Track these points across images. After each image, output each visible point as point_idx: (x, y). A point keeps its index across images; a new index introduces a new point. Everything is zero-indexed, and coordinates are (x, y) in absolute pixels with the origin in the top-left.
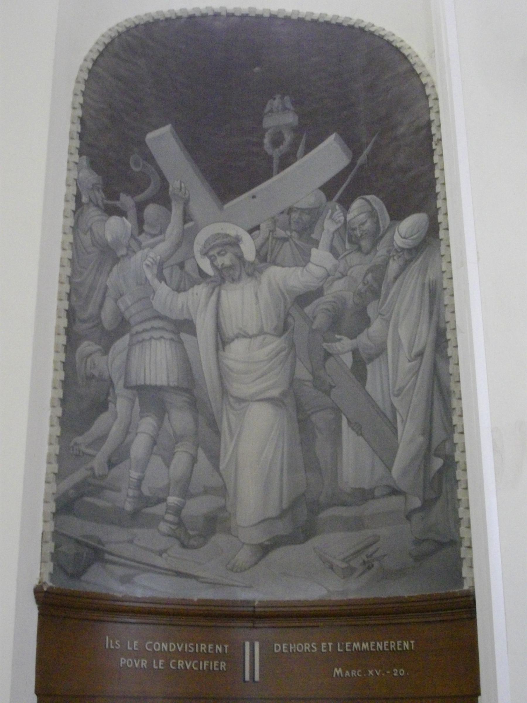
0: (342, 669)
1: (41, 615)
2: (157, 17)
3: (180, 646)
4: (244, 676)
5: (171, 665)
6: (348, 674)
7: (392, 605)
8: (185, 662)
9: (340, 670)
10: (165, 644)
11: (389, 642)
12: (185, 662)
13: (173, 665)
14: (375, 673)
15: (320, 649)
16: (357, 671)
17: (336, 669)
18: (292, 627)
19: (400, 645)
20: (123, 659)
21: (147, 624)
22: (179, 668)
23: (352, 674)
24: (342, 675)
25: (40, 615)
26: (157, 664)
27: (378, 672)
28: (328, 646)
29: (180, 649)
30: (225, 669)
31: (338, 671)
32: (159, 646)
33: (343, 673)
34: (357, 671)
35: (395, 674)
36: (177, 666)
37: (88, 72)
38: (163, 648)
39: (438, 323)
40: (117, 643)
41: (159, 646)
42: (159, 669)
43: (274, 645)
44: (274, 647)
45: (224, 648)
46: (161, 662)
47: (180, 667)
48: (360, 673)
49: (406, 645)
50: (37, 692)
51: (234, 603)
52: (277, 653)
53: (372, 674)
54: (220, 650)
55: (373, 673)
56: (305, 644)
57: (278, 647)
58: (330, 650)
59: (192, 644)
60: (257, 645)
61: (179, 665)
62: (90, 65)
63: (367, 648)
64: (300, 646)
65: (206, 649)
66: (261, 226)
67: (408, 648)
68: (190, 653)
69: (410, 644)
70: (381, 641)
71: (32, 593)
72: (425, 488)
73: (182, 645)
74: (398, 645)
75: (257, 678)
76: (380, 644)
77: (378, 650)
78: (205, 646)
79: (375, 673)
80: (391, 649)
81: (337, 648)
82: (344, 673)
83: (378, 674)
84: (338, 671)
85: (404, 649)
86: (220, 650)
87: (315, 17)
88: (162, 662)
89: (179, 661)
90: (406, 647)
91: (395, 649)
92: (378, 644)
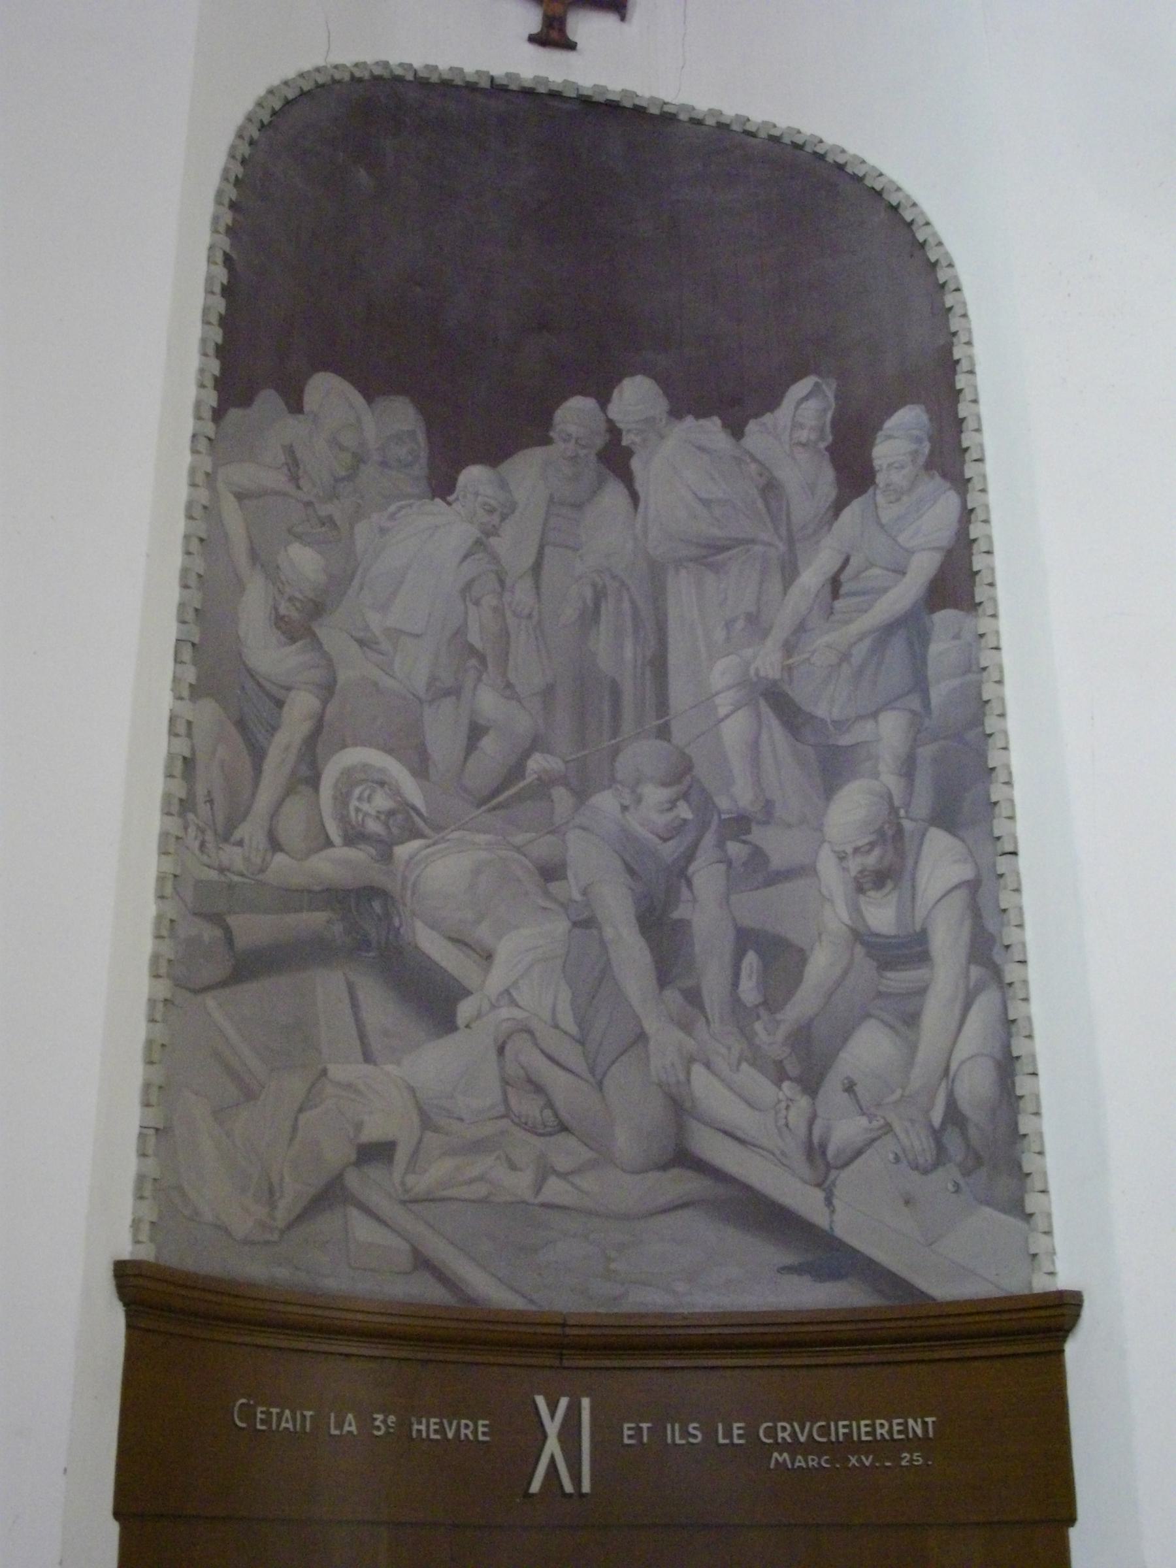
4: (561, 1487)
8: (793, 1427)
10: (916, 1422)
12: (793, 1427)
16: (820, 1458)
20: (467, 1422)
22: (879, 1437)
23: (811, 1463)
26: (728, 1434)
28: (639, 1430)
29: (450, 1435)
33: (790, 1460)
34: (820, 1458)
35: (904, 1463)
40: (692, 1431)
48: (827, 1461)
49: (914, 1425)
54: (919, 1431)
55: (857, 1461)
58: (645, 1439)
60: (677, 1426)
61: (879, 1431)
65: (887, 1432)
68: (693, 1444)
69: (925, 1424)
70: (792, 1420)
77: (911, 1435)
78: (887, 1425)
79: (859, 1460)
80: (879, 1437)
81: (329, 1428)
83: (867, 1464)
85: (911, 1435)
86: (919, 1431)
92: (911, 1422)
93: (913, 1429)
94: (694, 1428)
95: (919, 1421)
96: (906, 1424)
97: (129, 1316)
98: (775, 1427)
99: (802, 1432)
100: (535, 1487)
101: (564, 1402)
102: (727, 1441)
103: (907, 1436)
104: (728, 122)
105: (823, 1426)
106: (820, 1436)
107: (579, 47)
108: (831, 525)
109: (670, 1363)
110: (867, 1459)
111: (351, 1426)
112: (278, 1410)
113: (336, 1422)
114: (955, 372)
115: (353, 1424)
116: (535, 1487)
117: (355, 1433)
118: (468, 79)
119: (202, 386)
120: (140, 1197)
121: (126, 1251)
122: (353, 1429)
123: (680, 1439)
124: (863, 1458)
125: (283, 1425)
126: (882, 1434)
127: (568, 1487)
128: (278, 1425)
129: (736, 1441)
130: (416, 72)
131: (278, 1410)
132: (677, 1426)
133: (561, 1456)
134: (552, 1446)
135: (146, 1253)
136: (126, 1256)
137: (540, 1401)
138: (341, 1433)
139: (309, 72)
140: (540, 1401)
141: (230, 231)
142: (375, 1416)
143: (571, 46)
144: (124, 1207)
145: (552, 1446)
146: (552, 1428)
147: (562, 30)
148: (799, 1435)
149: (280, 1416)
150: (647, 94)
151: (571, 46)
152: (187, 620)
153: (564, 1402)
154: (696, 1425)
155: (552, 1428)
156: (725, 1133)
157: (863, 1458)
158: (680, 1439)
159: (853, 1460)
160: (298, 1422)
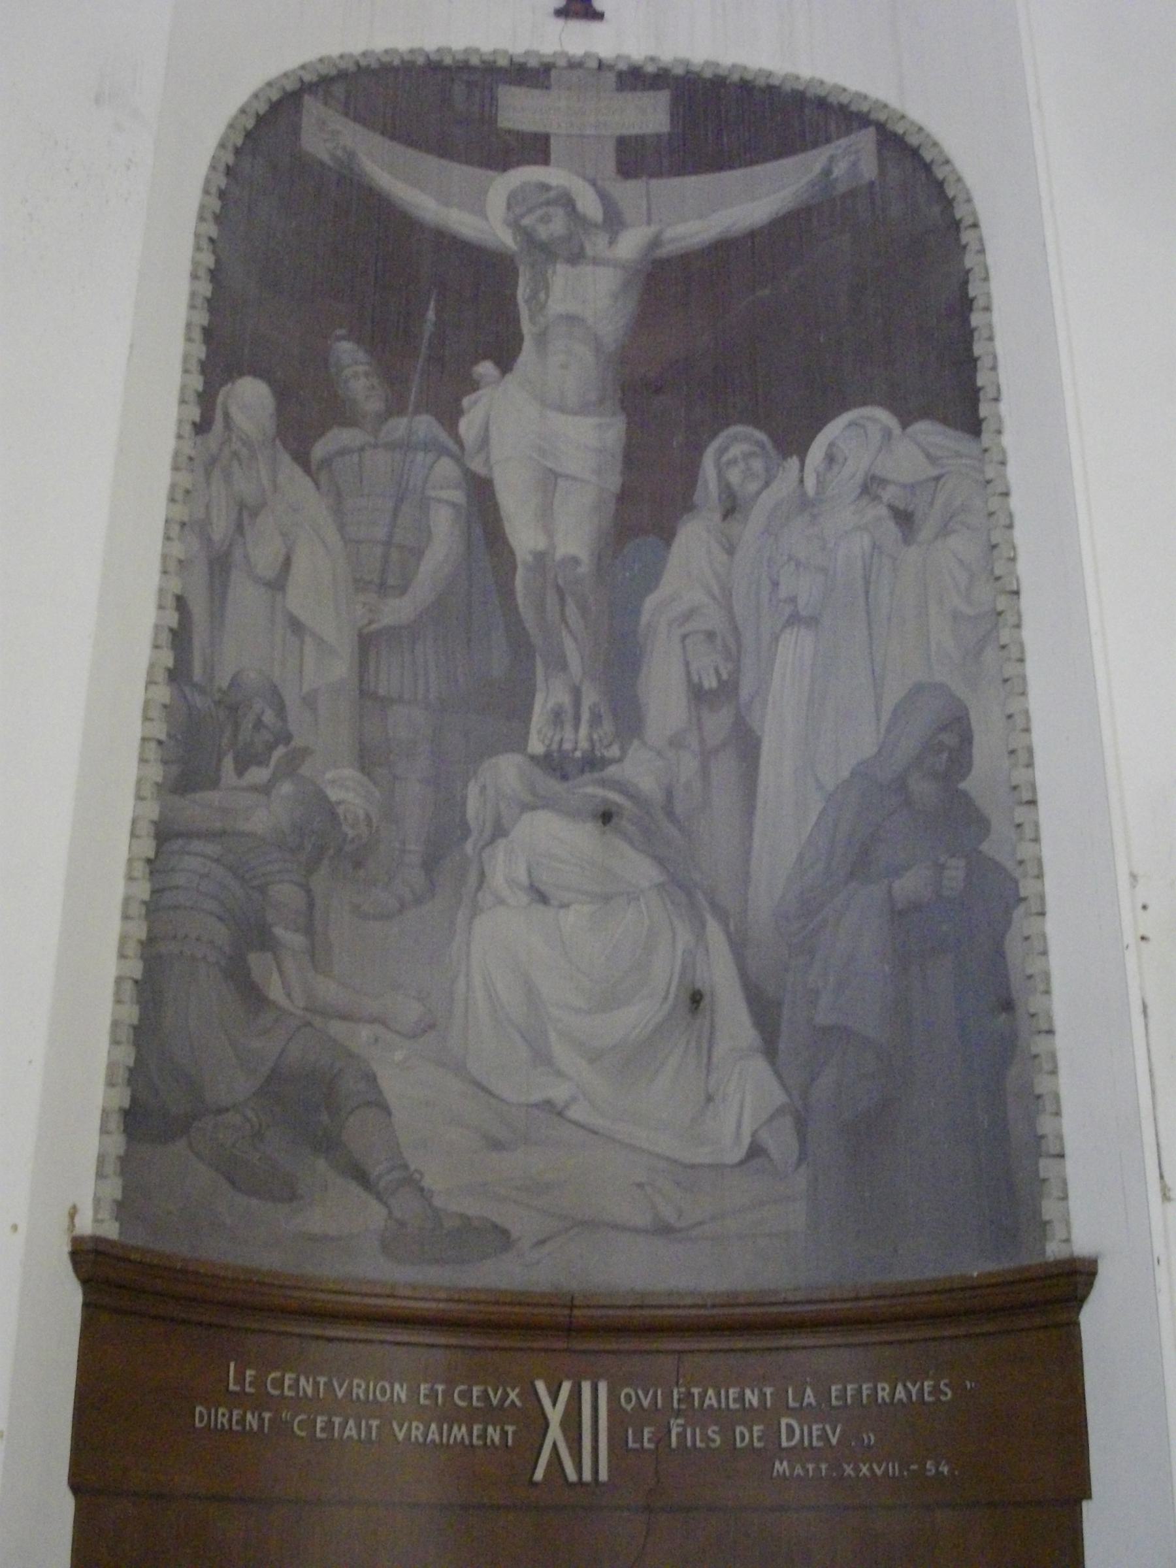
0: (789, 1461)
2: (343, 65)
5: (456, 1395)
6: (354, 1433)
9: (785, 1463)
11: (861, 1387)
14: (485, 1397)
15: (577, 1419)
17: (777, 1464)
19: (819, 1433)
21: (915, 1318)
24: (787, 1474)
25: (86, 1305)
26: (639, 1438)
37: (244, 133)
38: (395, 1394)
41: (798, 1432)
43: (779, 1424)
44: (734, 1433)
45: (763, 1395)
46: (647, 1432)
49: (751, 1397)
50: (76, 1486)
55: (868, 1469)
59: (713, 1445)
60: (603, 1387)
62: (250, 123)
63: (784, 1471)
66: (901, 429)
67: (255, 1427)
74: (475, 1433)
75: (603, 1476)
78: (888, 1390)
79: (871, 1469)
82: (792, 1468)
87: (775, 82)
88: (290, 1379)
90: (252, 1423)
91: (227, 1427)
93: (304, 1389)
94: (714, 1432)
95: (498, 1428)
99: (834, 1433)
100: (539, 1475)
101: (566, 1387)
102: (637, 1446)
103: (485, 1444)
104: (726, 73)
106: (300, 1429)
107: (606, 15)
108: (818, 476)
110: (880, 1468)
114: (971, 310)
116: (539, 1475)
118: (485, 58)
122: (812, 1400)
127: (572, 1476)
128: (702, 1402)
130: (428, 56)
131: (700, 1390)
132: (603, 1387)
133: (606, 1447)
134: (555, 1433)
137: (541, 1386)
140: (541, 1386)
141: (219, 219)
143: (598, 16)
145: (555, 1433)
146: (555, 1415)
148: (831, 1436)
149: (703, 1396)
150: (782, 73)
151: (598, 16)
153: (566, 1387)
154: (716, 1428)
155: (555, 1415)
156: (1158, 1145)
158: (235, 1384)
160: (723, 1400)
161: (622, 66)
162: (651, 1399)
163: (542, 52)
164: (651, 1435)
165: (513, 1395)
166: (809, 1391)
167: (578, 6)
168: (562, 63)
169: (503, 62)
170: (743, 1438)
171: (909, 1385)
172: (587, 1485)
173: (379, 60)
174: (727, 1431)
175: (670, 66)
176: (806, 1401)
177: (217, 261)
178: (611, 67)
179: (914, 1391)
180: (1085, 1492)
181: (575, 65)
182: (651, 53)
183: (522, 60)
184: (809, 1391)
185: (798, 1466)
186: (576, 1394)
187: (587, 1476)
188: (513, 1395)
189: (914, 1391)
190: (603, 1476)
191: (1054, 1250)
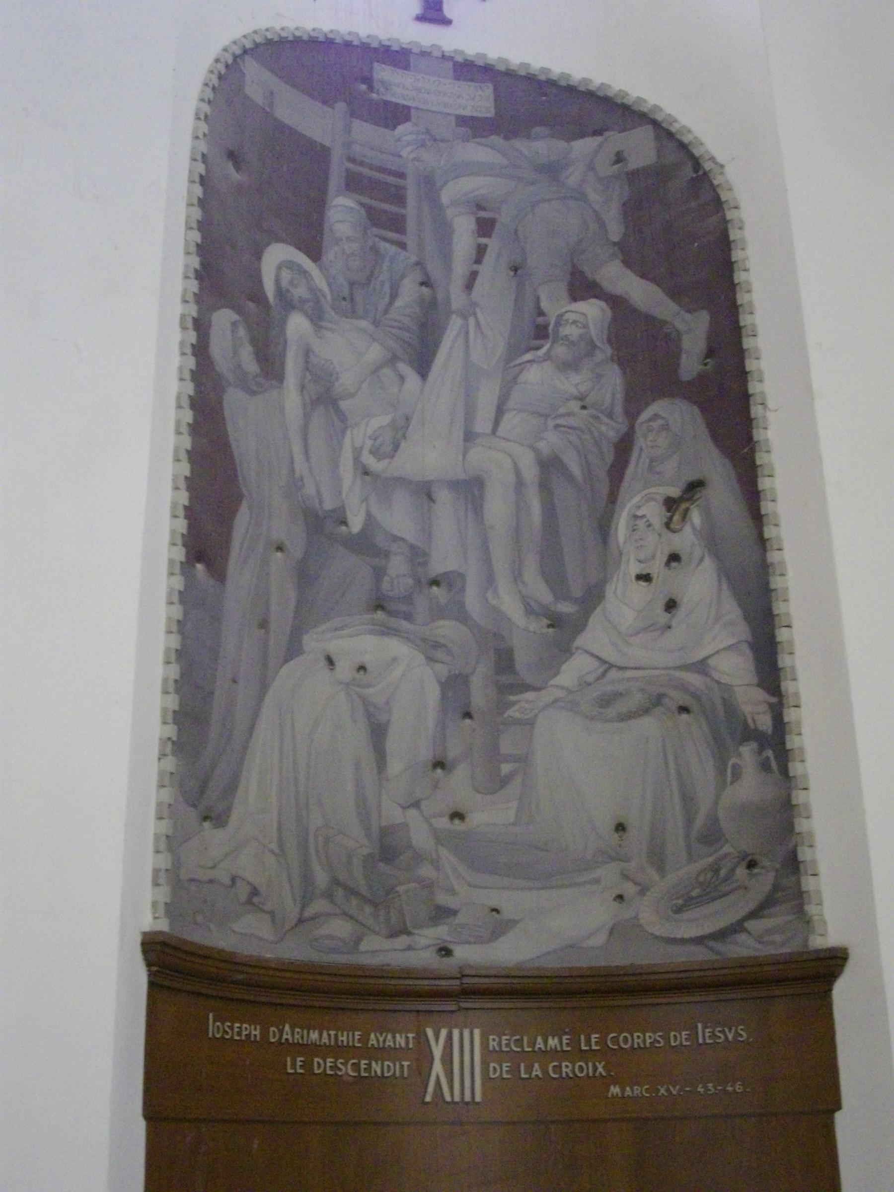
1: (153, 986)
3: (730, 1031)
6: (392, 1044)
7: (603, 979)
13: (612, 1043)
18: (488, 1009)
22: (564, 1075)
23: (636, 1092)
26: (294, 1065)
27: (674, 1090)
30: (258, 1038)
31: (615, 1090)
32: (392, 1067)
36: (561, 1072)
39: (749, 933)
41: (392, 1067)
42: (591, 1050)
44: (313, 1062)
47: (566, 1073)
51: (362, 967)
52: (673, 1047)
53: (666, 1094)
56: (635, 1035)
57: (495, 1068)
61: (564, 1070)
64: (625, 1038)
65: (571, 1071)
71: (138, 949)
72: (552, 888)
73: (444, 1033)
74: (504, 1042)
75: (478, 1098)
76: (400, 1044)
79: (668, 1090)
80: (564, 1075)
82: (623, 1090)
83: (675, 1093)
84: (615, 1090)
89: (564, 1064)
96: (369, 1065)
97: (151, 974)
98: (560, 1066)
100: (428, 1098)
105: (557, 1065)
107: (454, 23)
109: (730, 996)
111: (537, 1071)
112: (335, 1032)
113: (528, 1043)
115: (539, 1070)
117: (541, 1076)
119: (183, 354)
120: (156, 884)
121: (147, 921)
123: (586, 1046)
124: (671, 1087)
125: (323, 1041)
126: (566, 1072)
129: (594, 1047)
131: (335, 1032)
132: (477, 1032)
135: (163, 925)
136: (147, 929)
138: (530, 1076)
139: (249, 34)
141: (198, 276)
142: (708, 1085)
143: (447, 22)
144: (147, 894)
145: (438, 1068)
146: (437, 1051)
147: (440, 9)
151: (447, 22)
152: (178, 515)
153: (444, 1033)
157: (671, 1087)
159: (662, 1091)
161: (460, 59)
162: (445, 1047)
163: (402, 41)
164: (686, 1037)
165: (600, 1069)
166: (536, 1066)
167: (431, 14)
168: (415, 50)
169: (375, 45)
170: (274, 1036)
171: (378, 1035)
172: (457, 1103)
173: (309, 34)
174: (574, 1042)
175: (536, 73)
176: (534, 1073)
177: (208, 170)
178: (451, 58)
179: (381, 1039)
180: (837, 1105)
181: (425, 54)
182: (332, 28)
183: (388, 43)
184: (536, 1066)
185: (628, 1089)
186: (450, 1037)
187: (468, 1098)
188: (600, 1069)
189: (381, 1039)
190: (478, 1098)
191: (818, 942)
